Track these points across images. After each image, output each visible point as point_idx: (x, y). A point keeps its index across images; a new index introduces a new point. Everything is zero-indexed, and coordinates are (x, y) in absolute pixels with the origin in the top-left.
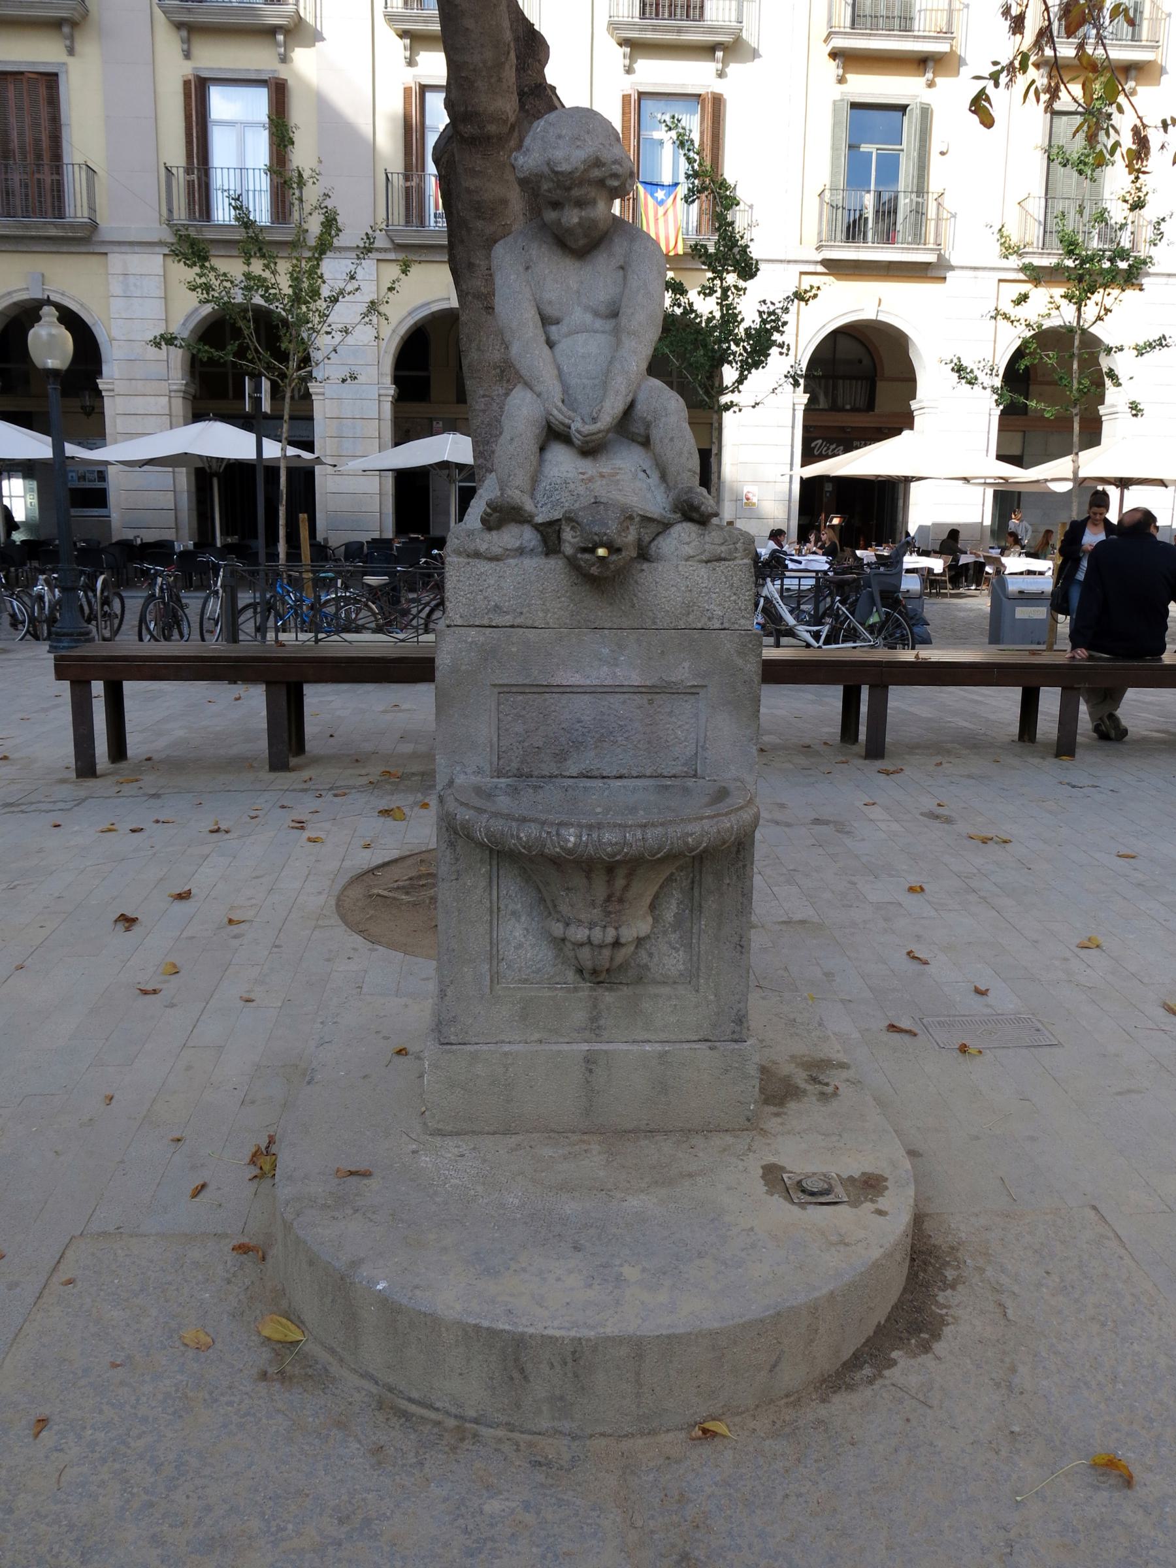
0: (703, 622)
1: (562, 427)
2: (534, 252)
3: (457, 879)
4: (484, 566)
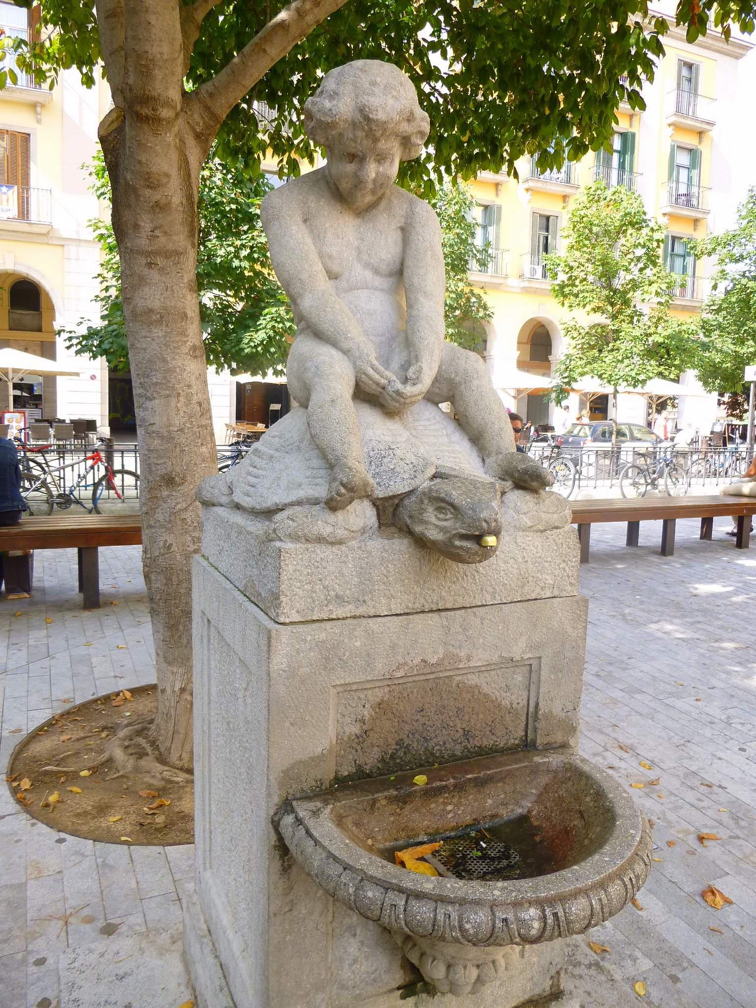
0: (536, 592)
1: (374, 387)
2: (313, 205)
3: (291, 910)
4: (323, 552)
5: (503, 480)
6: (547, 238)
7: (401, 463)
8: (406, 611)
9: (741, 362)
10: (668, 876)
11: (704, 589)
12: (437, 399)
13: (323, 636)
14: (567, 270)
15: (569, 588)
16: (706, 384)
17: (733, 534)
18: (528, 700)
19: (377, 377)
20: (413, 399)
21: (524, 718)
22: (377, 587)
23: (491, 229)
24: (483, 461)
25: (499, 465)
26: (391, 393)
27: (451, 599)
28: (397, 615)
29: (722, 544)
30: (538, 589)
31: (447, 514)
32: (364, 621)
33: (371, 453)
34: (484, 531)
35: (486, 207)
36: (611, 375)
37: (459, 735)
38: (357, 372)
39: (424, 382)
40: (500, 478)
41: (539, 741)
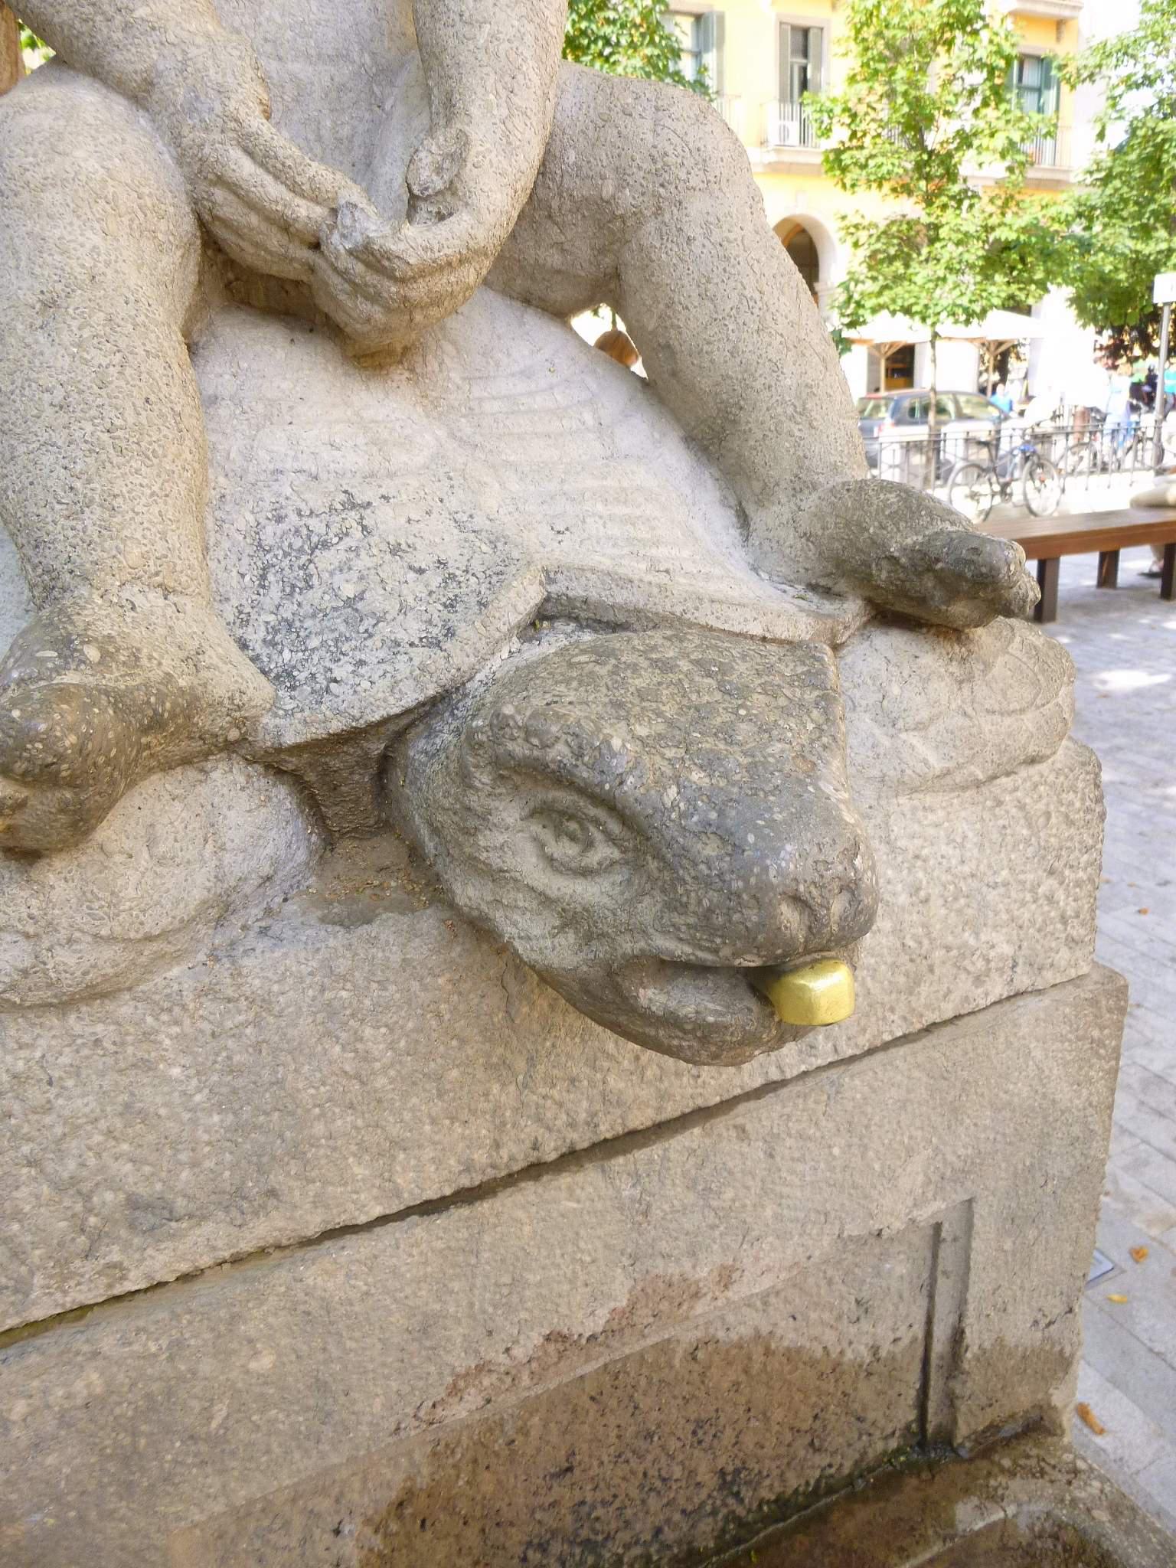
0: (955, 997)
1: (275, 241)
5: (827, 593)
6: (804, 70)
7: (394, 569)
8: (465, 1182)
9: (1146, 269)
10: (1144, 1337)
11: (1122, 680)
12: (558, 294)
13: (91, 1381)
14: (848, 121)
15: (1063, 955)
16: (1082, 311)
17: (1151, 575)
18: (929, 1322)
19: (273, 191)
20: (441, 283)
21: (914, 1377)
22: (319, 1128)
23: (710, 59)
24: (744, 520)
25: (807, 536)
26: (346, 263)
27: (646, 1093)
28: (429, 1208)
29: (1137, 595)
30: (964, 985)
31: (589, 845)
32: (279, 1277)
33: (270, 534)
34: (790, 951)
35: (698, 18)
36: (926, 306)
37: (704, 1494)
38: (191, 181)
39: (482, 202)
40: (813, 587)
41: (962, 1431)
